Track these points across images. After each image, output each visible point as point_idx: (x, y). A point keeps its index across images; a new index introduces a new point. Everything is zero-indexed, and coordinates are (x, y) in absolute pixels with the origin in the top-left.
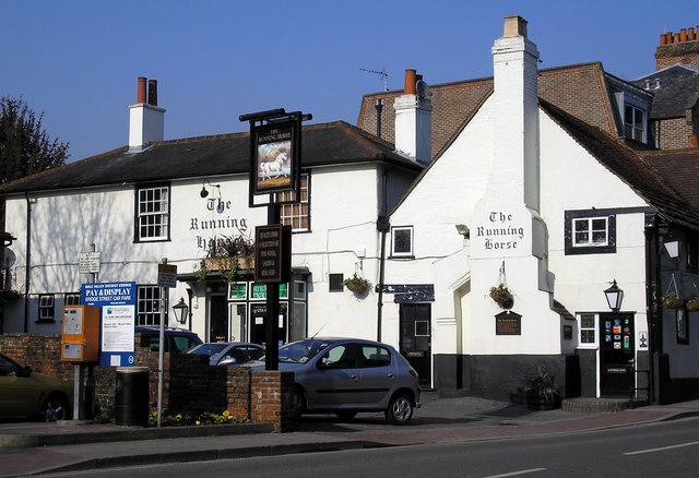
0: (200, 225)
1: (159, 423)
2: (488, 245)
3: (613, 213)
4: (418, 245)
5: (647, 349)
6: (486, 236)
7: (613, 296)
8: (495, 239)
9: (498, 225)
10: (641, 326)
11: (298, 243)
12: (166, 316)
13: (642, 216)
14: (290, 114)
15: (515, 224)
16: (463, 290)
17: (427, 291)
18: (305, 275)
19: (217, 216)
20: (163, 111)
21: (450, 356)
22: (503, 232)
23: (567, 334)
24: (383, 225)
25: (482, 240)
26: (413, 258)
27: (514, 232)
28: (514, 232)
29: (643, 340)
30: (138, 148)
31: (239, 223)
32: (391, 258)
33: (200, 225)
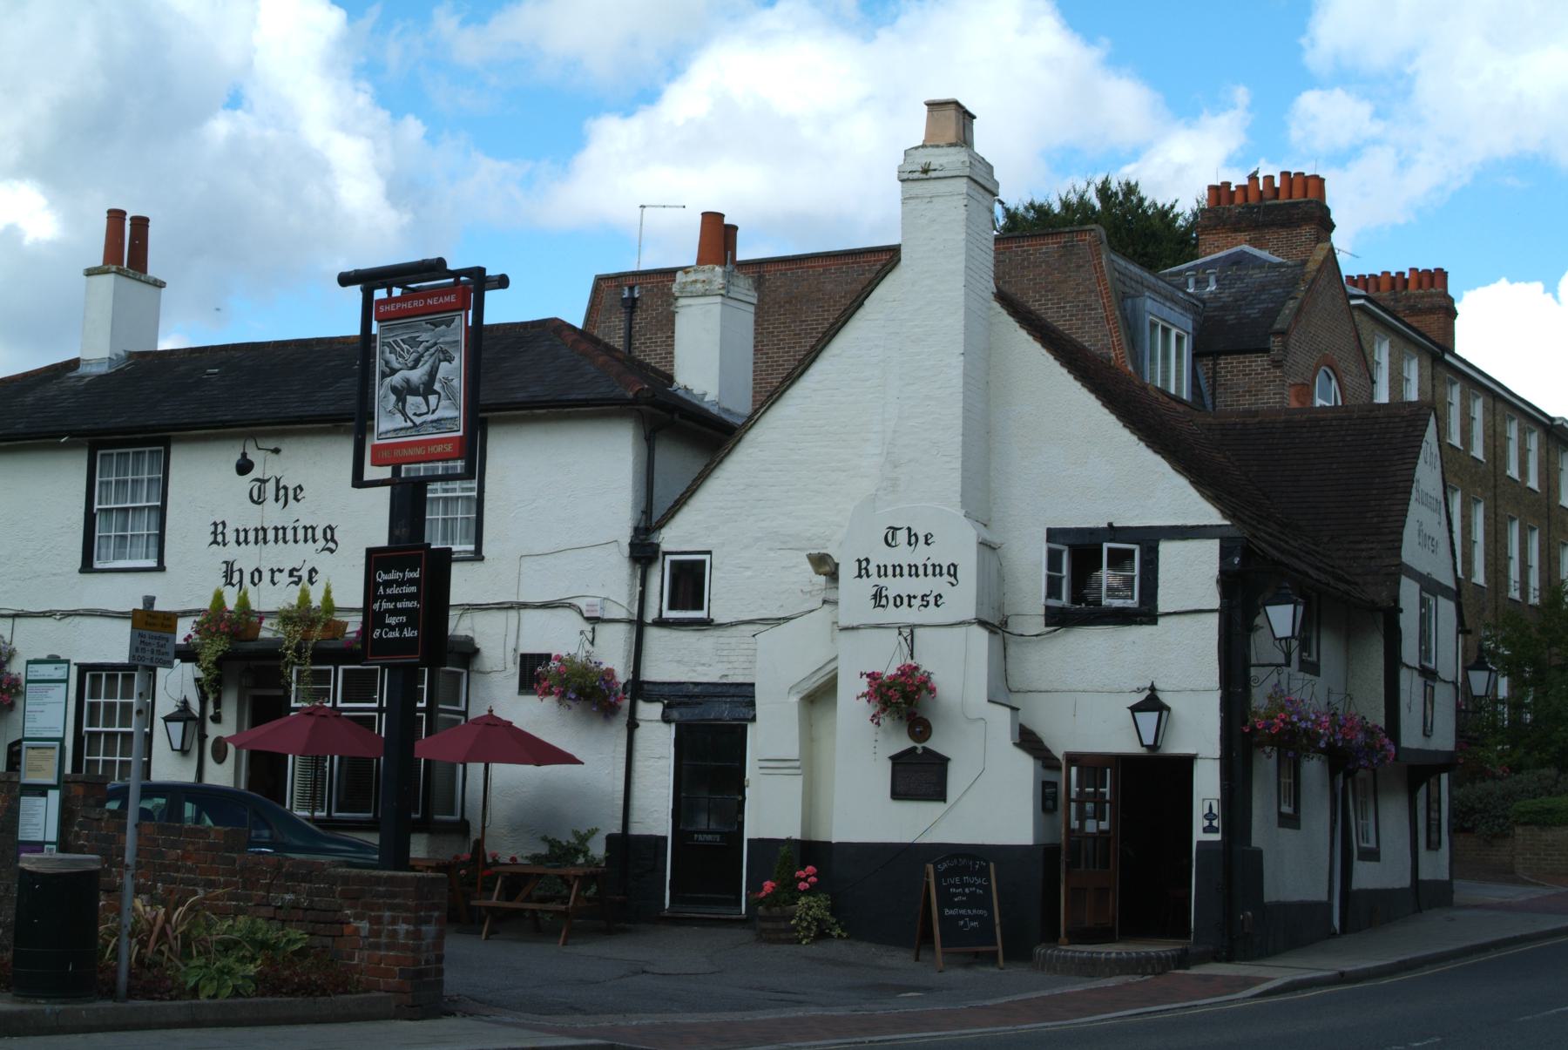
0: (231, 536)
1: (147, 455)
2: (878, 597)
3: (1150, 539)
4: (721, 599)
5: (1217, 837)
6: (874, 579)
7: (1148, 720)
8: (894, 586)
9: (903, 554)
10: (1207, 786)
11: (464, 584)
12: (149, 738)
13: (1212, 547)
14: (456, 274)
15: (940, 554)
16: (821, 695)
17: (743, 695)
18: (467, 653)
19: (272, 515)
20: (159, 284)
21: (789, 842)
22: (914, 571)
23: (1047, 798)
24: (643, 552)
25: (867, 586)
26: (707, 623)
27: (937, 570)
28: (937, 570)
29: (1209, 816)
30: (100, 362)
31: (319, 534)
32: (661, 623)
33: (231, 536)
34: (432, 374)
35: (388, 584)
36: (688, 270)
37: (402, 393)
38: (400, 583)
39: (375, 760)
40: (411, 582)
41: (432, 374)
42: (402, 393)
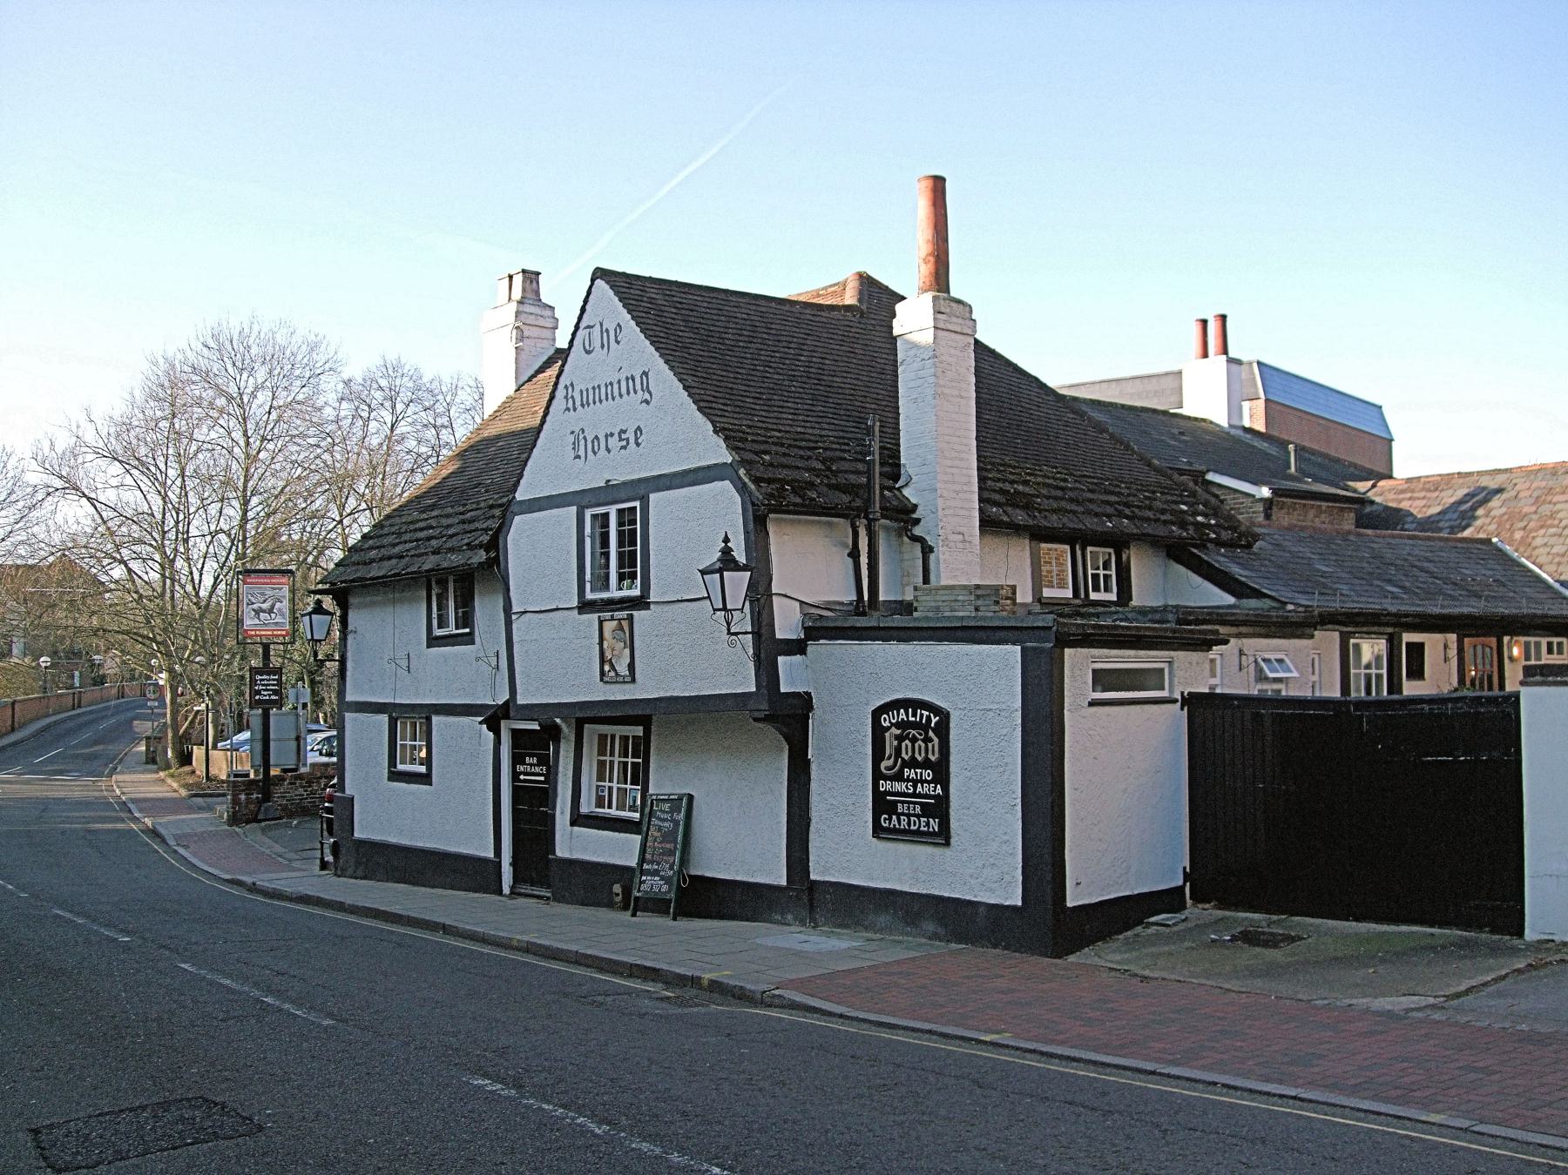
34: (273, 606)
35: (261, 680)
36: (534, 283)
37: (258, 612)
38: (269, 680)
39: (467, 630)
40: (274, 680)
41: (273, 606)
42: (258, 612)
